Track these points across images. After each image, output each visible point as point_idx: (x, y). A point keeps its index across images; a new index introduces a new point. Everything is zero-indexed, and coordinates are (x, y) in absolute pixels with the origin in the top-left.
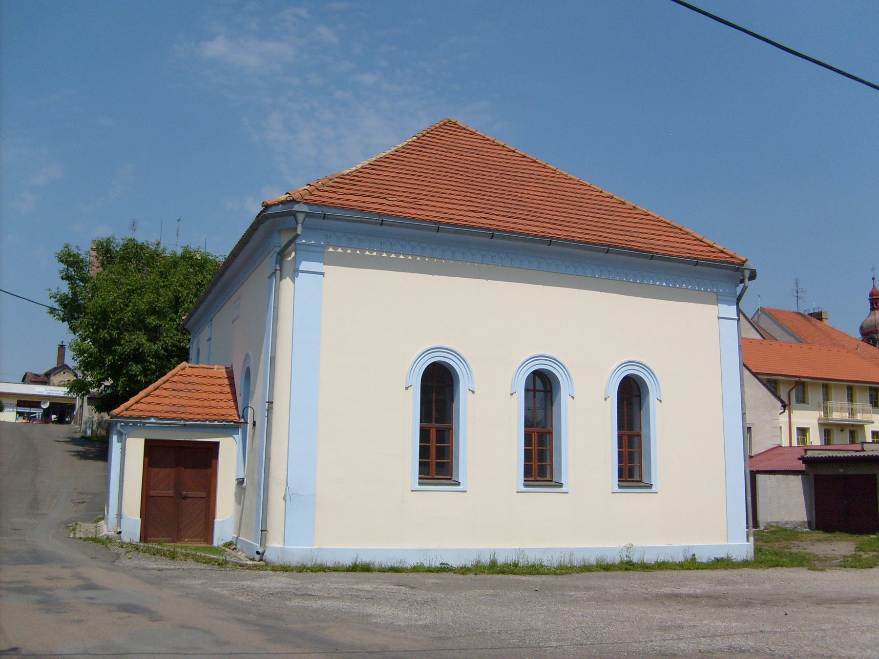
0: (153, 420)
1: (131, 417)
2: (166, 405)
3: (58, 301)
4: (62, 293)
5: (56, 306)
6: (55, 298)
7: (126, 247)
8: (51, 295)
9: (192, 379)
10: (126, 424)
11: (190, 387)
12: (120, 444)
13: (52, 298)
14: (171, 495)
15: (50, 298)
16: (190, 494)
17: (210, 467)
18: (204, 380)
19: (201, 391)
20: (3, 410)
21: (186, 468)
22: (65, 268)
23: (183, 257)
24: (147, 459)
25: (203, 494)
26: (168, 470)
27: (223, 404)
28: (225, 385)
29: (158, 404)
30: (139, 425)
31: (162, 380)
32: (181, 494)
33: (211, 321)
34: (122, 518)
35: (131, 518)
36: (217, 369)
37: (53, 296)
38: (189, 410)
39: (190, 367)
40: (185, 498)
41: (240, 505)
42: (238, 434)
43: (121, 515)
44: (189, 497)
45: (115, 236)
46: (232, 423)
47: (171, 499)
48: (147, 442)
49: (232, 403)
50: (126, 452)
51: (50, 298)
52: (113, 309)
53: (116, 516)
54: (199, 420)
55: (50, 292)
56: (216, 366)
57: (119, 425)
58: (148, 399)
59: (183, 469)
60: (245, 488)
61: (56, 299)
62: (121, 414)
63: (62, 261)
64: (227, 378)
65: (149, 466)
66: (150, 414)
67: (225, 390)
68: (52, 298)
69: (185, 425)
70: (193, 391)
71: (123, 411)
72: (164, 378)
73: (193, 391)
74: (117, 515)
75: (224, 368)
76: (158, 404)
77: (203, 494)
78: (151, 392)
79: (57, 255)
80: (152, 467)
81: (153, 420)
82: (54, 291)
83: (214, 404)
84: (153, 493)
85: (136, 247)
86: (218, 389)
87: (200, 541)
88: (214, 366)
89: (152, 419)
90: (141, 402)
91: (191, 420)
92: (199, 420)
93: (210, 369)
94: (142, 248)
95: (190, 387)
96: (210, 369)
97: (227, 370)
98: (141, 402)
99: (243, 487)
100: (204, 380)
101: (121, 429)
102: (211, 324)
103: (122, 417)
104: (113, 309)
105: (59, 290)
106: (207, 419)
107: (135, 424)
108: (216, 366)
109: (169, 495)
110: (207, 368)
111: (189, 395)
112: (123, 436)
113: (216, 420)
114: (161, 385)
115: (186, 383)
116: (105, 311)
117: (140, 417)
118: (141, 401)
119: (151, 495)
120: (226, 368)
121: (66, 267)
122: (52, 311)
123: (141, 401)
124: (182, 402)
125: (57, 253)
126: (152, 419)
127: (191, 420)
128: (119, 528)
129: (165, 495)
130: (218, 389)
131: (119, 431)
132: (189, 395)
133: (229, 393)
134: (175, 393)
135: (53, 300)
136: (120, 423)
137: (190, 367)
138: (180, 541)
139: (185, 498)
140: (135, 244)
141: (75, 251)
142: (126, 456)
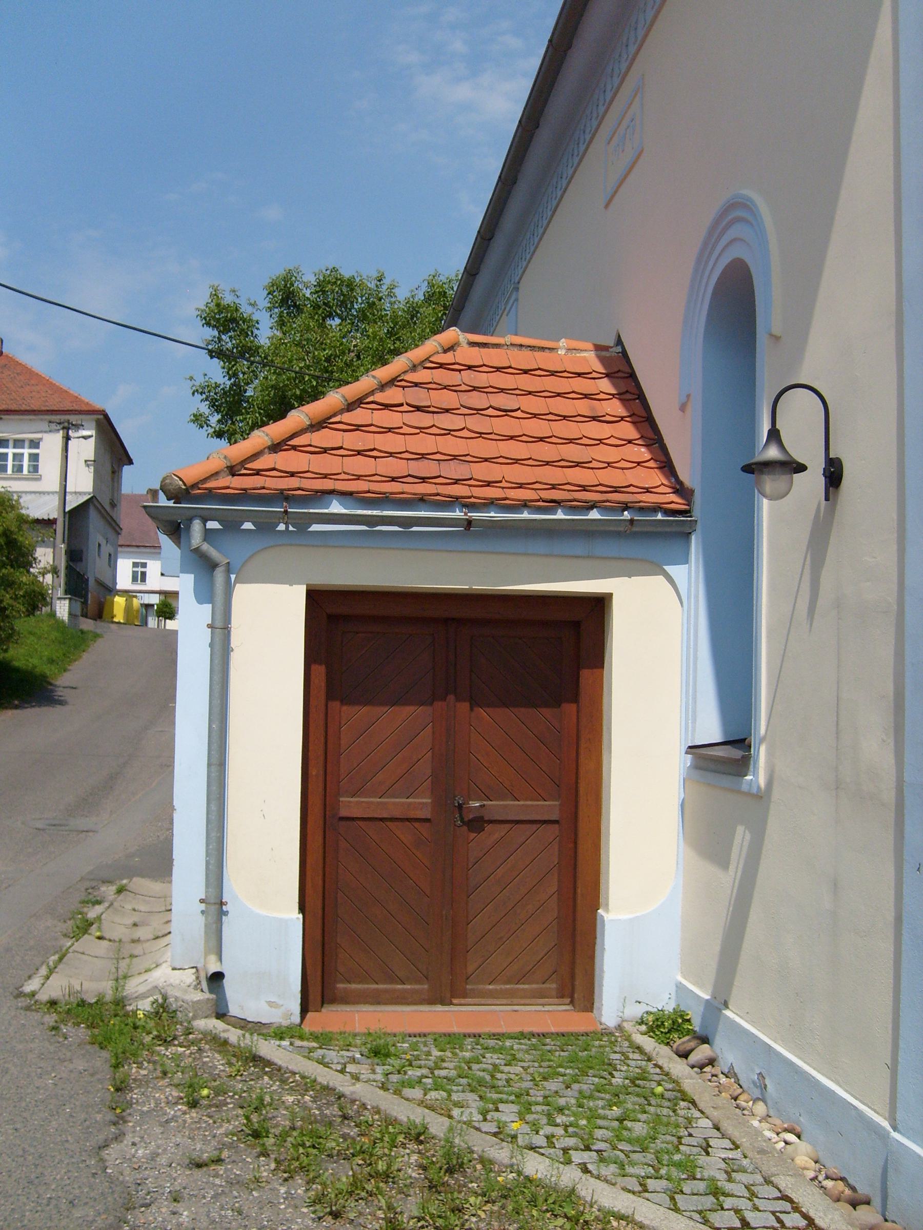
0: (336, 507)
1: (244, 496)
2: (391, 454)
3: (206, 399)
4: (213, 382)
5: (204, 408)
6: (201, 393)
7: (321, 287)
8: (194, 388)
9: (481, 379)
10: (231, 525)
11: (478, 400)
12: (208, 607)
13: (196, 393)
14: (425, 813)
15: (193, 394)
16: (498, 807)
17: (575, 698)
18: (526, 382)
19: (518, 414)
20: (174, 616)
21: (475, 702)
22: (214, 337)
23: (429, 298)
24: (320, 670)
25: (549, 808)
26: (407, 711)
27: (611, 454)
28: (602, 396)
29: (359, 453)
30: (282, 527)
31: (374, 377)
32: (460, 806)
33: (517, 289)
34: (226, 913)
35: (264, 912)
36: (569, 350)
37: (197, 391)
38: (482, 471)
39: (473, 344)
40: (477, 824)
41: (724, 863)
42: (686, 561)
43: (222, 904)
44: (491, 822)
45: (301, 269)
46: (660, 517)
47: (423, 828)
48: (315, 598)
49: (643, 449)
50: (233, 644)
51: (193, 394)
52: (298, 392)
53: (203, 907)
54: (525, 505)
55: (191, 383)
56: (563, 343)
57: (197, 525)
58: (321, 438)
59: (464, 706)
60: (761, 798)
61: (204, 396)
62: (211, 484)
63: (208, 324)
64: (607, 375)
65: (331, 695)
66: (328, 484)
67: (609, 411)
68: (196, 393)
69: (469, 523)
70: (490, 412)
71: (217, 474)
72: (383, 373)
73: (490, 412)
74: (202, 901)
75: (591, 346)
76: (359, 453)
77: (549, 808)
78: (334, 415)
79: (199, 313)
80: (344, 701)
81: (336, 507)
82: (200, 380)
83: (573, 452)
84: (350, 805)
85: (339, 282)
86: (583, 407)
87: (541, 995)
88: (559, 340)
89: (335, 502)
90: (294, 448)
91: (490, 503)
92: (525, 505)
93: (543, 349)
94: (350, 284)
95: (478, 400)
96: (543, 349)
97: (604, 353)
98: (294, 448)
99: (745, 787)
100: (526, 382)
101: (205, 547)
102: (517, 300)
103: (211, 495)
104: (298, 392)
105: (207, 379)
106: (557, 503)
107: (265, 527)
108: (563, 340)
109: (412, 814)
110: (532, 348)
111: (477, 424)
112: (219, 575)
113: (592, 506)
114: (372, 393)
115: (464, 388)
116: (284, 397)
117: (283, 496)
118: (293, 442)
119: (344, 813)
120: (598, 348)
121: (216, 333)
122: (199, 420)
123: (293, 442)
124: (451, 445)
125: (198, 309)
126: (335, 502)
127: (490, 503)
128: (213, 958)
129: (397, 814)
130: (583, 407)
131: (197, 551)
132: (477, 424)
133: (622, 418)
134: (424, 420)
135: (198, 397)
136: (205, 521)
137: (473, 344)
138: (464, 995)
139: (477, 824)
140: (337, 279)
141: (228, 299)
142: (233, 656)
